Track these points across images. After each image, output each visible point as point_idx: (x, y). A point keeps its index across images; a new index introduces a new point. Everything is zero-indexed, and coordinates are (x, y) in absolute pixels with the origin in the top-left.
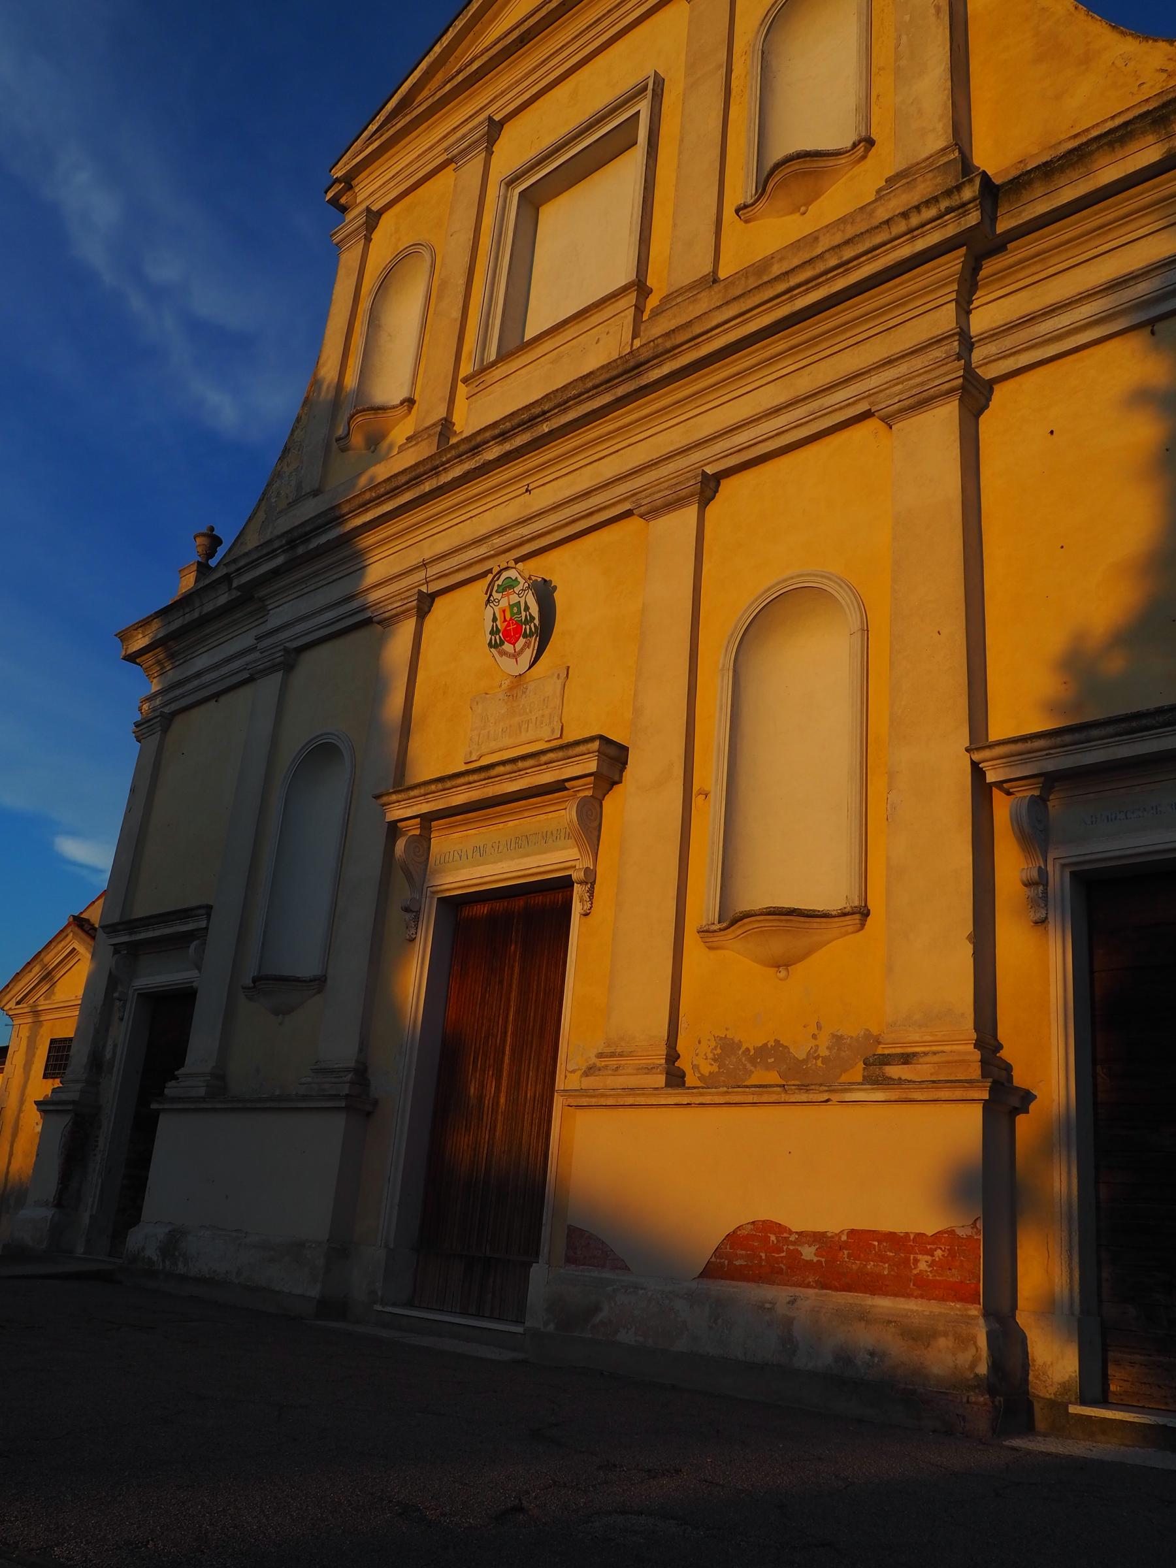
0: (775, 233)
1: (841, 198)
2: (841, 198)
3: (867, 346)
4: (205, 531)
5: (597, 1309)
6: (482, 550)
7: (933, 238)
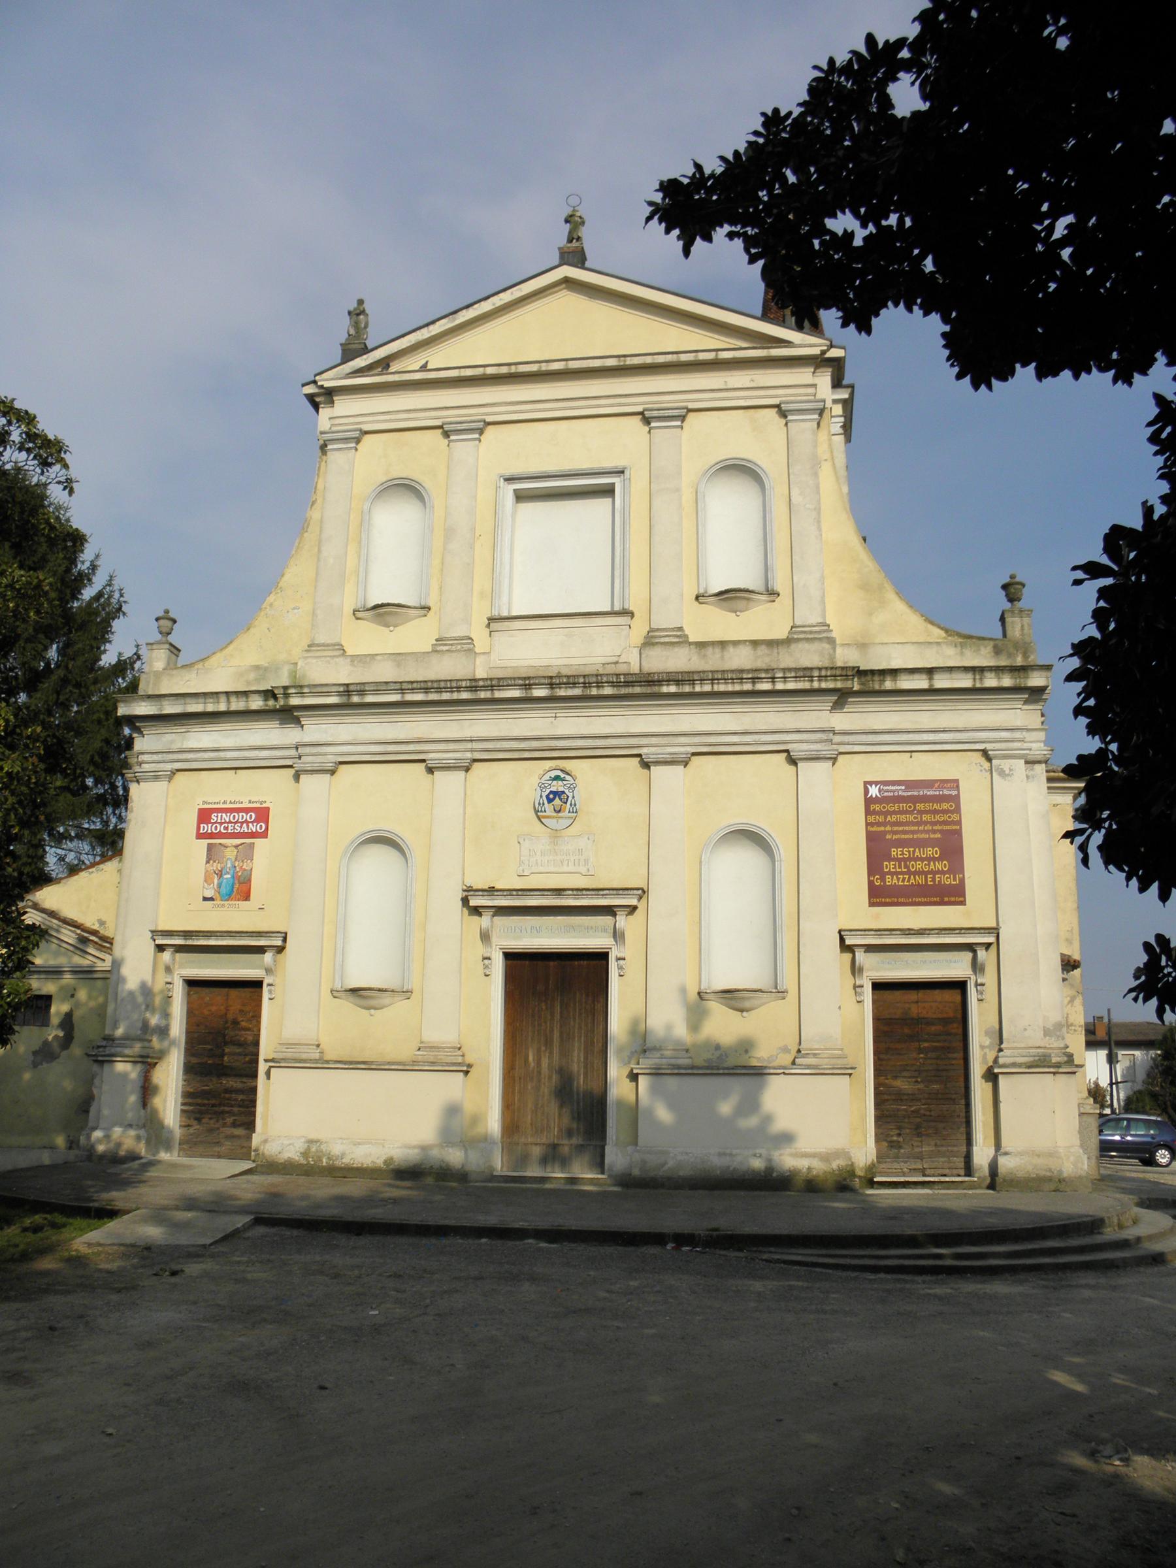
0: (368, 639)
1: (414, 636)
2: (414, 636)
3: (764, 728)
4: (161, 614)
5: (666, 1163)
6: (523, 745)
7: (830, 685)
